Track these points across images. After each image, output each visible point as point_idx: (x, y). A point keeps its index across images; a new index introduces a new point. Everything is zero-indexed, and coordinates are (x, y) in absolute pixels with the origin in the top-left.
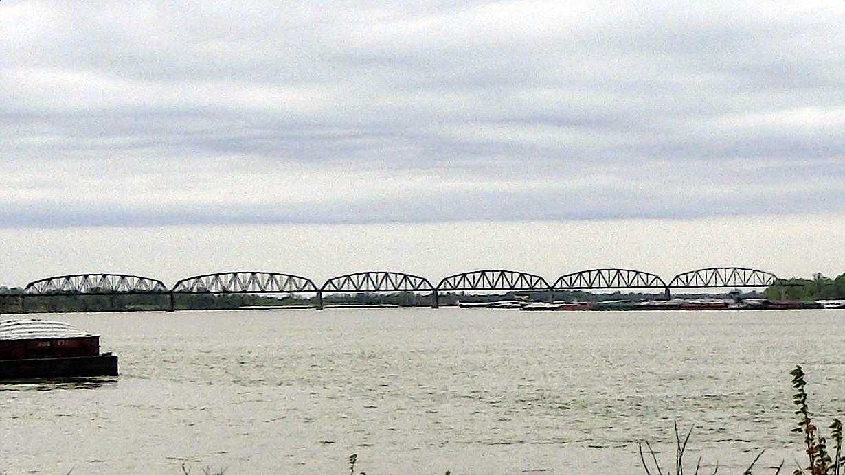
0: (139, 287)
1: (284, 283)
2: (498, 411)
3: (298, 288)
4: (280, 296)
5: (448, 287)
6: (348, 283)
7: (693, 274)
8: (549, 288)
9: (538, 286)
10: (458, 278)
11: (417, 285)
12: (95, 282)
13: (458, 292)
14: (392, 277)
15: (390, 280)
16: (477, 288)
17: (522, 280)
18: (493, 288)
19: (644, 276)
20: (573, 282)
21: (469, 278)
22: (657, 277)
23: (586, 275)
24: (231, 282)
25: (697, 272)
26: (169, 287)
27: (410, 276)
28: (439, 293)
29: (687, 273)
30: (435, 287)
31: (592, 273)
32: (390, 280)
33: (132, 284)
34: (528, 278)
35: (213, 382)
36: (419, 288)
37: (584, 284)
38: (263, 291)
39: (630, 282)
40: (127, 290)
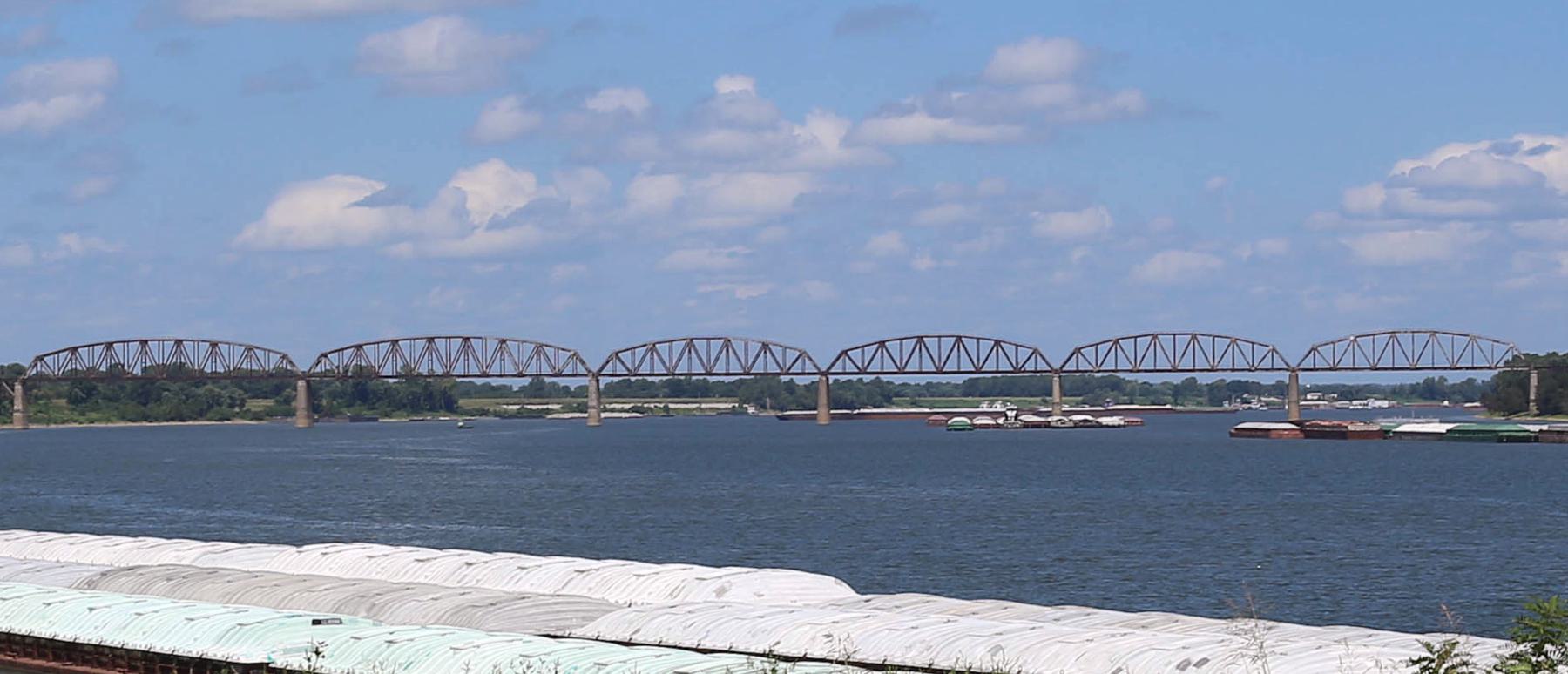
0: (244, 366)
1: (610, 364)
2: (837, 639)
3: (782, 369)
4: (517, 384)
5: (850, 368)
6: (652, 358)
7: (1111, 343)
8: (1052, 370)
9: (1030, 366)
10: (870, 350)
11: (788, 367)
12: (162, 355)
13: (867, 378)
14: (971, 345)
15: (739, 360)
16: (907, 370)
17: (1116, 348)
18: (940, 372)
19: (1247, 347)
20: (1099, 363)
21: (660, 351)
22: (1035, 351)
23: (1128, 345)
24: (386, 359)
25: (1117, 342)
26: (303, 366)
27: (257, 348)
28: (832, 378)
29: (863, 347)
30: (824, 369)
31: (1336, 344)
32: (739, 360)
33: (231, 359)
34: (1010, 350)
35: (88, 611)
36: (791, 371)
37: (1123, 364)
38: (484, 375)
39: (981, 365)
40: (221, 370)
